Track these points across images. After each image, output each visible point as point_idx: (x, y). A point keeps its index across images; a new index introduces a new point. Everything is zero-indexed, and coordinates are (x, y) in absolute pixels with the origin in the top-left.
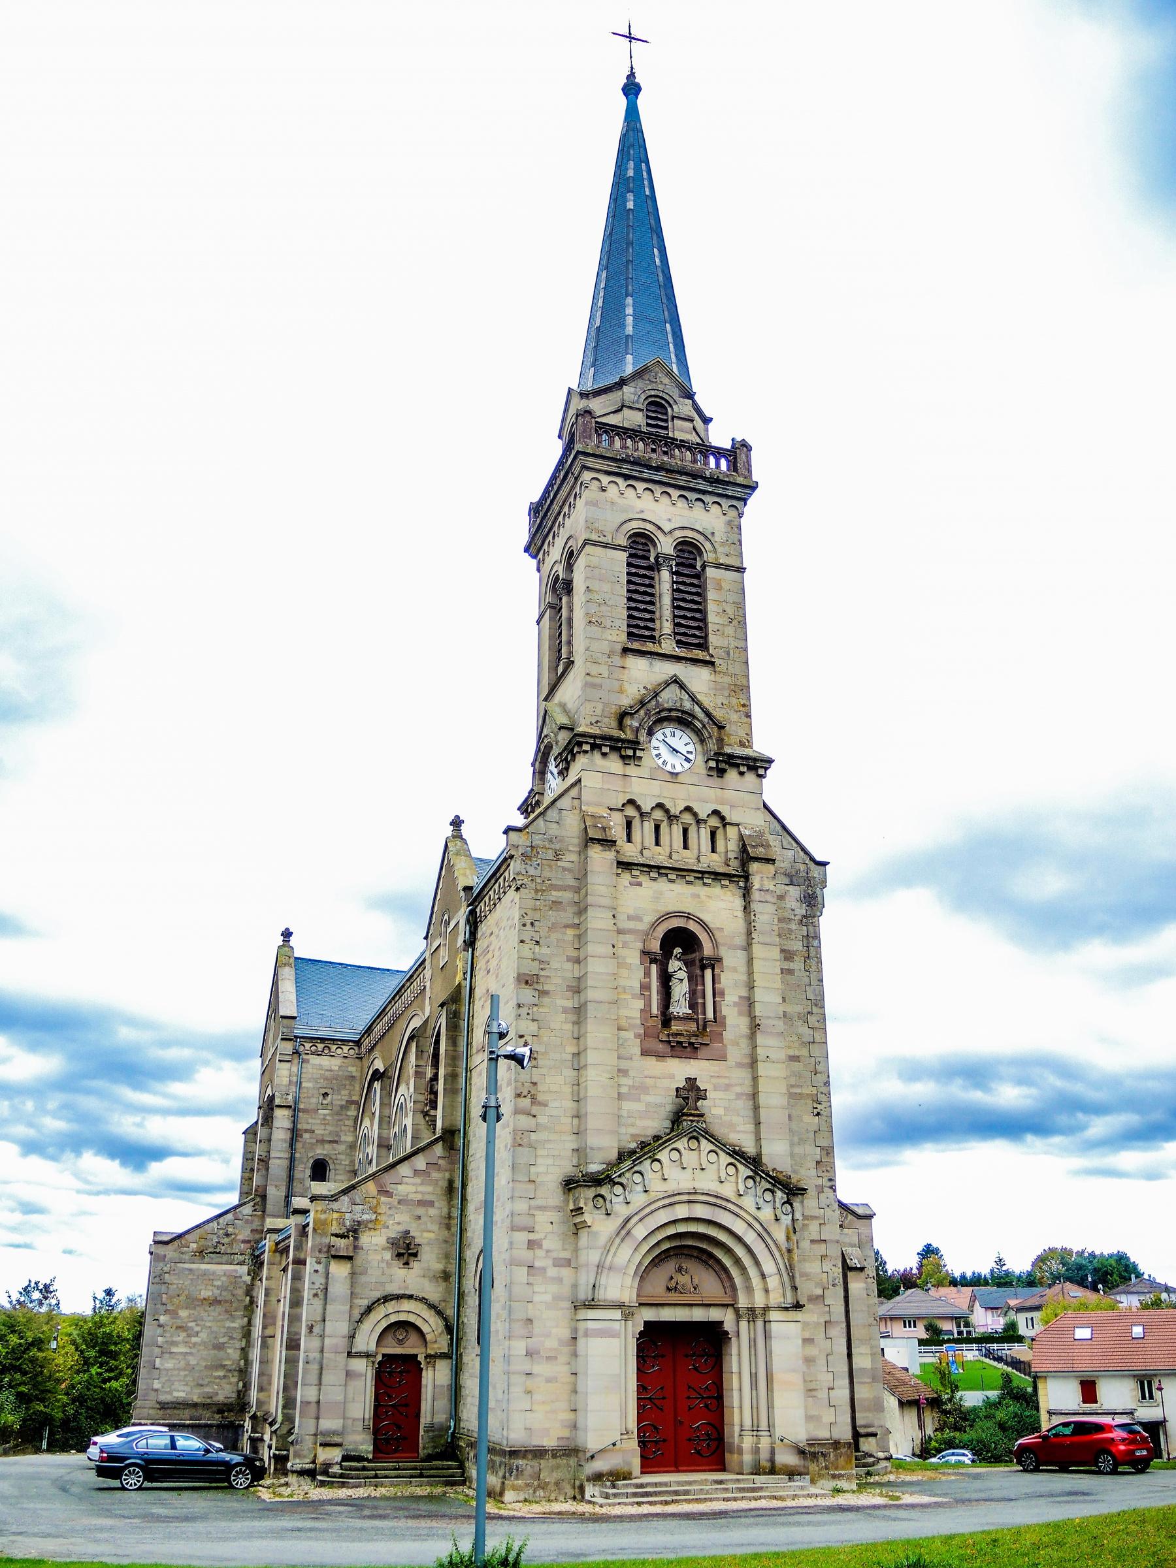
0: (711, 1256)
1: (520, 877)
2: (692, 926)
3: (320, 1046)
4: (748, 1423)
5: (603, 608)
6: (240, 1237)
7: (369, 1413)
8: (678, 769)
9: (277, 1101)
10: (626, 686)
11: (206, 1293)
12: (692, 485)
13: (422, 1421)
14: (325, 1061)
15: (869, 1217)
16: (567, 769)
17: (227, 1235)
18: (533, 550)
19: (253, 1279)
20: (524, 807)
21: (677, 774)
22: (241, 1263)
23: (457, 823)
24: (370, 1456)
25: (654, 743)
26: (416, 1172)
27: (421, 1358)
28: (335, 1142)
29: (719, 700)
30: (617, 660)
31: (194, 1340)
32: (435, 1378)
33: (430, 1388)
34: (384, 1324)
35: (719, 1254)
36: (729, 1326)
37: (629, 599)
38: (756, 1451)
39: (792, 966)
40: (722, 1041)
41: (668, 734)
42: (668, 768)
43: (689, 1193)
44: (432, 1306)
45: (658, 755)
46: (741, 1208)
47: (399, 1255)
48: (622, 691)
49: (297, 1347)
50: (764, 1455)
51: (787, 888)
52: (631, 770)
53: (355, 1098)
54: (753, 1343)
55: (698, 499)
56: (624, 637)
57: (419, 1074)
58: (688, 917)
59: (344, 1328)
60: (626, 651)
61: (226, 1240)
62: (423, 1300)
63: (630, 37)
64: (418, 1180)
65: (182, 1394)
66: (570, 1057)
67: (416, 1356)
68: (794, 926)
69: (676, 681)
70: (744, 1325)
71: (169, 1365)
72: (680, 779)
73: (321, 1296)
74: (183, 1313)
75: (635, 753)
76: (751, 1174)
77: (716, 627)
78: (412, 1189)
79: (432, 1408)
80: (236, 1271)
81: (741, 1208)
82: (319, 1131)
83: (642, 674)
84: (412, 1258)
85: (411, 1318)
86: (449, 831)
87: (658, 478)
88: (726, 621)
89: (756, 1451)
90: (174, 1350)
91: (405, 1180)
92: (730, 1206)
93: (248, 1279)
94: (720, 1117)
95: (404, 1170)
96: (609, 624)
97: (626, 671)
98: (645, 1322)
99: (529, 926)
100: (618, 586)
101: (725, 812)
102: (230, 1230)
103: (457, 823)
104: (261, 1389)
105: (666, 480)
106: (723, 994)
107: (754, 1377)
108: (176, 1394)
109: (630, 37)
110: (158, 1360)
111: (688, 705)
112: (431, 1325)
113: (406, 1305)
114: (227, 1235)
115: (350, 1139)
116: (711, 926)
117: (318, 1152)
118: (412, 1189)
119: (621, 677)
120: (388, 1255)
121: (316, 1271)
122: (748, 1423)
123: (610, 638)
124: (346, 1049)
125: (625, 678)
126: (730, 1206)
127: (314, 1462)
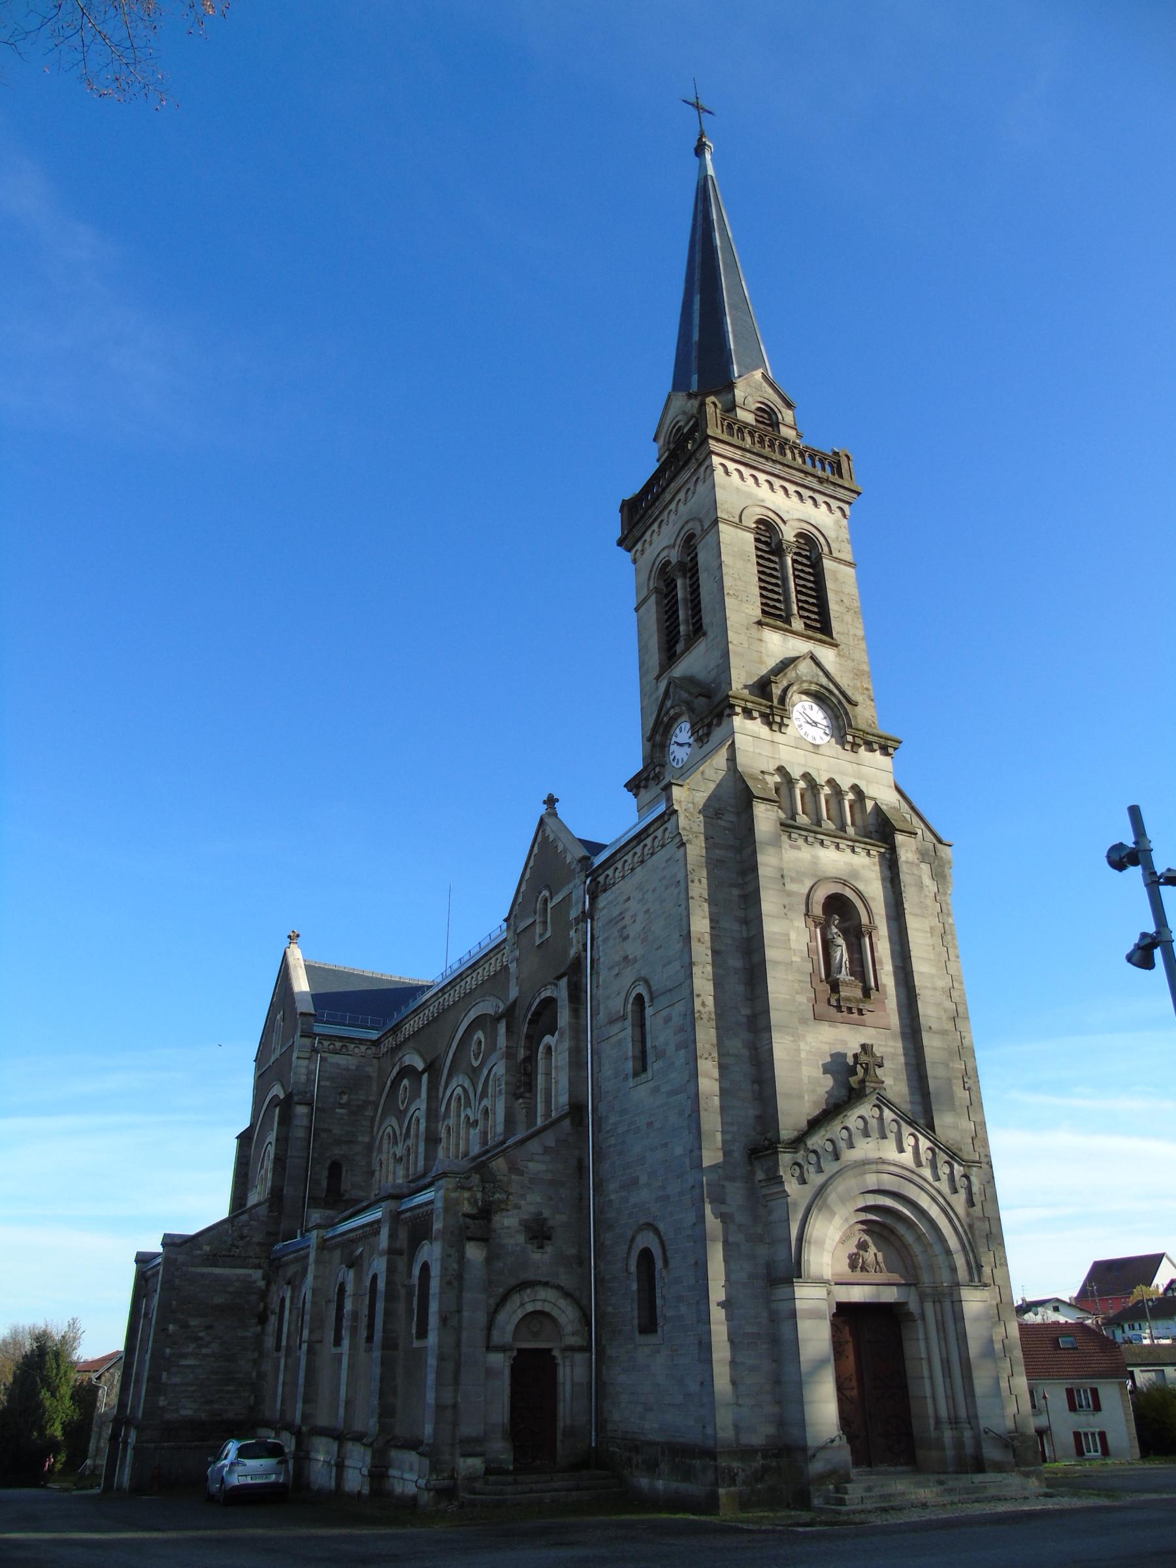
0: (892, 1231)
2: (848, 893)
3: (338, 1045)
4: (944, 1413)
5: (739, 583)
6: (255, 1240)
7: (507, 1419)
9: (296, 1099)
10: (765, 659)
11: (218, 1300)
12: (806, 483)
13: (560, 1424)
14: (341, 1060)
16: (708, 735)
17: (242, 1237)
18: (629, 542)
19: (268, 1285)
20: (633, 784)
21: (818, 746)
22: (258, 1267)
23: (551, 801)
24: (511, 1467)
26: (547, 1150)
27: (556, 1353)
28: (351, 1142)
31: (204, 1351)
32: (571, 1374)
33: (568, 1387)
34: (520, 1314)
35: (901, 1229)
36: (913, 1307)
37: (760, 580)
38: (959, 1444)
40: (885, 1010)
41: (807, 707)
44: (567, 1295)
45: (800, 726)
47: (533, 1238)
48: (761, 662)
49: (395, 1347)
50: (969, 1450)
52: (778, 737)
53: (372, 1098)
54: (941, 1326)
56: (759, 612)
57: (510, 1055)
58: (845, 883)
59: (481, 1317)
60: (760, 623)
61: (241, 1243)
62: (558, 1287)
63: (697, 106)
64: (547, 1158)
65: (190, 1412)
66: (744, 1020)
67: (550, 1350)
69: (813, 658)
70: (929, 1307)
71: (176, 1380)
72: (821, 751)
73: (456, 1284)
74: (193, 1322)
78: (543, 1167)
79: (569, 1406)
80: (250, 1275)
82: (337, 1130)
84: (546, 1242)
85: (547, 1308)
86: (542, 809)
87: (776, 472)
89: (959, 1444)
90: (184, 1362)
91: (536, 1157)
93: (262, 1284)
95: (534, 1146)
96: (745, 599)
100: (749, 565)
101: (863, 788)
102: (245, 1232)
103: (551, 801)
104: (306, 1400)
107: (946, 1363)
108: (183, 1412)
109: (697, 106)
110: (164, 1375)
111: (824, 681)
112: (566, 1314)
113: (543, 1293)
114: (242, 1237)
115: (367, 1139)
117: (336, 1151)
118: (543, 1167)
120: (521, 1239)
121: (449, 1256)
122: (944, 1413)
124: (363, 1048)
125: (763, 650)
127: (452, 1477)
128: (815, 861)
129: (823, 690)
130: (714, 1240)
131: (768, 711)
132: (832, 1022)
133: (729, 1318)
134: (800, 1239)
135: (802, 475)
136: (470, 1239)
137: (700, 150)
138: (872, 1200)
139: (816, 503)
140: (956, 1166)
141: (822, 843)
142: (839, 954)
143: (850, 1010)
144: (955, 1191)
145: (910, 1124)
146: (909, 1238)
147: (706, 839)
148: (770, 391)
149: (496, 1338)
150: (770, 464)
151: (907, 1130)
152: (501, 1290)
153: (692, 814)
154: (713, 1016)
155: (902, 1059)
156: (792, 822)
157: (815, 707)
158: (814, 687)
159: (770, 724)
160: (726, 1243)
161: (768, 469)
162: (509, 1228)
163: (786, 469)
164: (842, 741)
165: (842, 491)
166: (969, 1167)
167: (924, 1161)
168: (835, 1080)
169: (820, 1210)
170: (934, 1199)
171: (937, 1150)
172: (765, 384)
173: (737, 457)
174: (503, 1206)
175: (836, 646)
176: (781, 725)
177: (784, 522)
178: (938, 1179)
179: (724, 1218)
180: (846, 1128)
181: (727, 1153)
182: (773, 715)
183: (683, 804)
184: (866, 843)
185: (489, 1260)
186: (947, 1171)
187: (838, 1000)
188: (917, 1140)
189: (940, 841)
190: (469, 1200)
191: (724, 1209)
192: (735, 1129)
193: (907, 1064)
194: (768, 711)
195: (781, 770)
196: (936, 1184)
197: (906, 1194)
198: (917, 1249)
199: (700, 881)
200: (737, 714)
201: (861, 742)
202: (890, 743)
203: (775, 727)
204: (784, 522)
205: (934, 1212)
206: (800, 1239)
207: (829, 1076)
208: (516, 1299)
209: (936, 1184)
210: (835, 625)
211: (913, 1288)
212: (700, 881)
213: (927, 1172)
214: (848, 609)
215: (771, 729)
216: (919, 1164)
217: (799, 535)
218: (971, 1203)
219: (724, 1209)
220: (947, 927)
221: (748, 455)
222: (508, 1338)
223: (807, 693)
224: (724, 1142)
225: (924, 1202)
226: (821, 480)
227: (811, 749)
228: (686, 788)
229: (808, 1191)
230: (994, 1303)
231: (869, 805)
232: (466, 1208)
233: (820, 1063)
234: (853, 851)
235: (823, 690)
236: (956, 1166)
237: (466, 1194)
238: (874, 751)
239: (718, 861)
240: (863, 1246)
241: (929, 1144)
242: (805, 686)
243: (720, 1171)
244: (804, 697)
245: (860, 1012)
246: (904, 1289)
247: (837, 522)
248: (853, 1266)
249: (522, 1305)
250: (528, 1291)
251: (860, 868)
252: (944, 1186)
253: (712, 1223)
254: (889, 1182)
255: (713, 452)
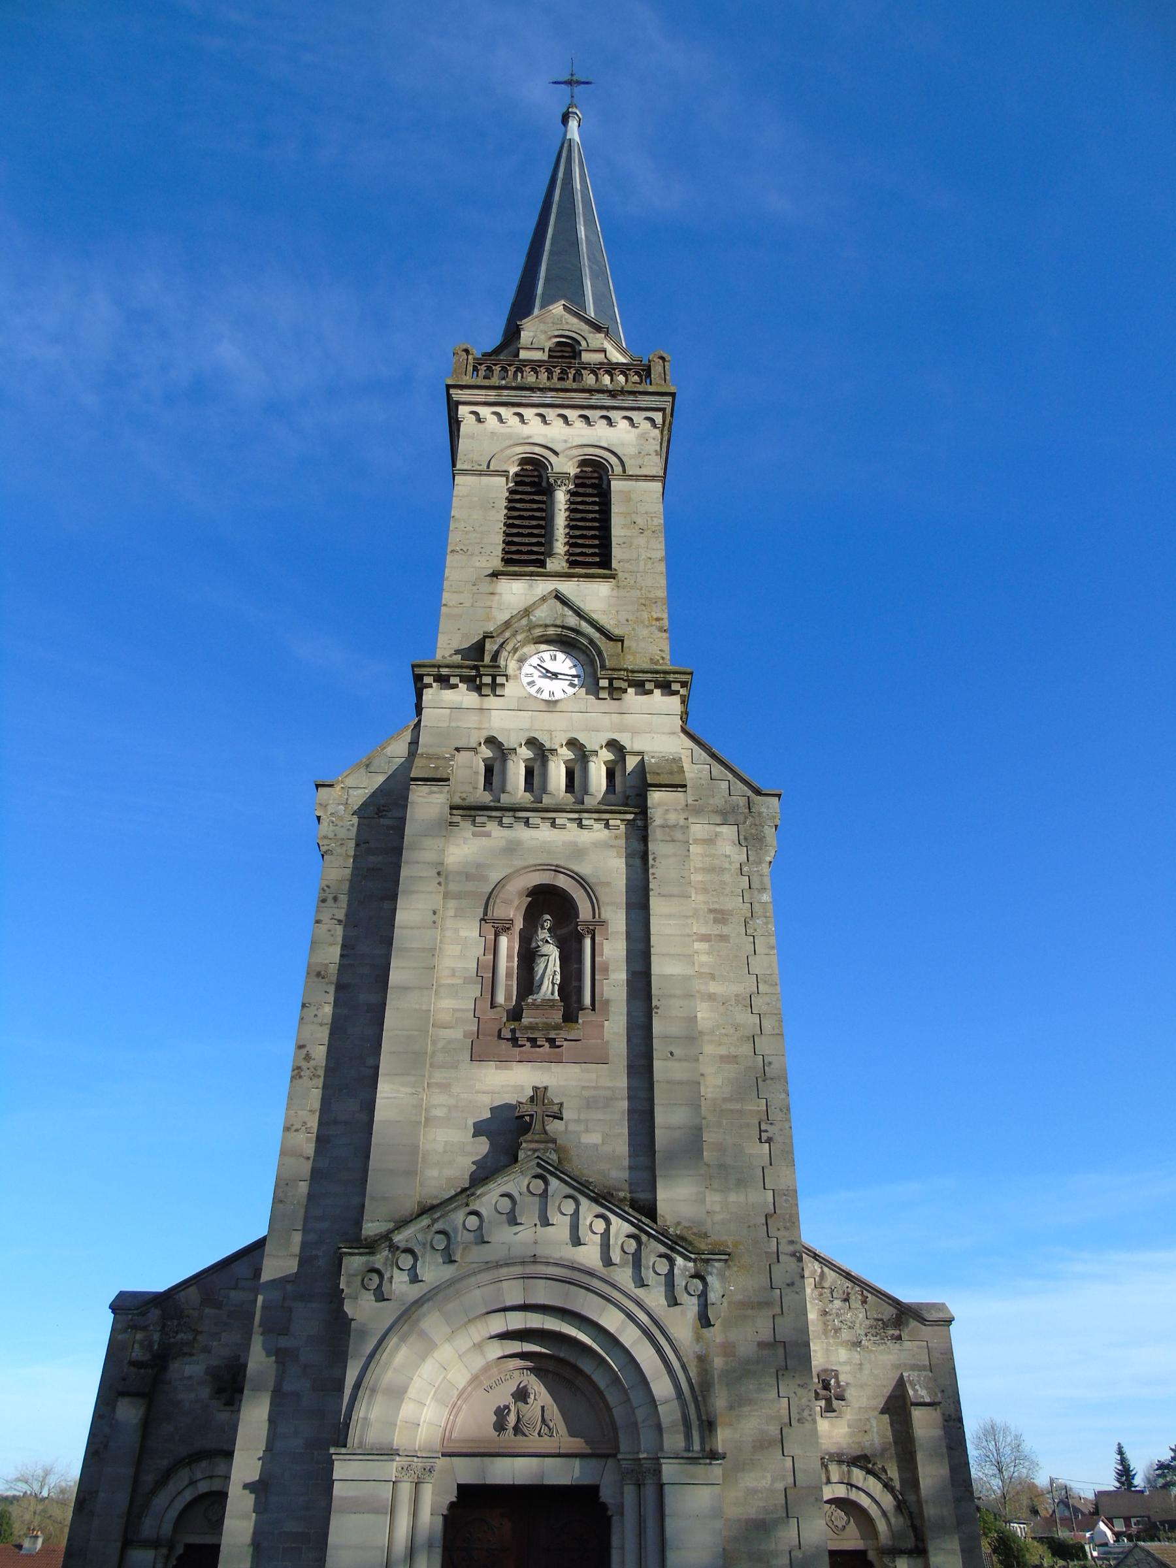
1: (326, 842)
2: (562, 882)
8: (559, 695)
12: (593, 402)
15: (949, 1321)
21: (556, 701)
25: (527, 668)
27: (872, 1556)
29: (623, 617)
30: (486, 586)
34: (188, 1496)
35: (586, 1366)
39: (726, 930)
42: (545, 696)
43: (523, 1263)
45: (532, 683)
46: (614, 1286)
48: (488, 618)
51: (718, 829)
52: (492, 702)
55: (603, 417)
58: (557, 870)
68: (727, 877)
69: (560, 598)
70: (629, 1491)
72: (560, 707)
75: (494, 680)
76: (632, 1230)
77: (621, 541)
81: (614, 1286)
83: (517, 593)
87: (548, 401)
88: (636, 532)
92: (596, 1283)
94: (596, 1146)
97: (496, 598)
98: (461, 1488)
99: (330, 902)
105: (559, 401)
106: (606, 970)
111: (572, 620)
116: (591, 880)
119: (488, 603)
120: (205, 1392)
123: (478, 564)
126: (596, 1283)
128: (512, 849)
129: (566, 632)
130: (257, 1389)
131: (473, 673)
132: (503, 1060)
133: (259, 1508)
134: (357, 1386)
135: (586, 395)
136: (123, 1394)
137: (565, 119)
138: (517, 1321)
139: (610, 421)
140: (680, 1261)
141: (527, 823)
142: (542, 966)
143: (533, 1041)
144: (673, 1302)
145: (595, 1200)
146: (601, 1381)
147: (357, 845)
148: (575, 320)
149: (147, 1527)
150: (538, 394)
151: (588, 1210)
152: (165, 1462)
153: (341, 818)
154: (321, 1072)
155: (625, 1105)
156: (582, 807)
157: (561, 656)
158: (551, 631)
159: (478, 689)
160: (278, 1397)
161: (536, 400)
162: (190, 1377)
163: (562, 394)
164: (593, 689)
165: (647, 398)
166: (707, 1261)
167: (616, 1256)
168: (491, 1144)
169: (403, 1339)
170: (630, 1316)
171: (644, 1238)
172: (567, 316)
173: (492, 399)
174: (186, 1350)
175: (613, 577)
176: (494, 686)
177: (556, 453)
178: (641, 1283)
179: (282, 1357)
180: (476, 1213)
181: (304, 1261)
182: (481, 676)
183: (330, 809)
184: (620, 812)
185: (146, 1425)
186: (663, 1267)
187: (513, 1031)
188: (608, 1222)
189: (758, 792)
190: (141, 1343)
191: (284, 1342)
192: (325, 1225)
193: (631, 1112)
194: (473, 673)
195: (491, 741)
196: (640, 1293)
197: (578, 1310)
198: (612, 1398)
199: (335, 899)
200: (430, 686)
201: (624, 685)
202: (671, 677)
203: (485, 691)
204: (556, 453)
205: (630, 1337)
206: (357, 1386)
207: (484, 1139)
208: (184, 1475)
209: (640, 1293)
210: (616, 552)
211: (610, 1462)
212: (335, 899)
213: (624, 1276)
214: (642, 531)
215: (481, 695)
216: (608, 1262)
217: (583, 463)
218: (704, 1320)
219: (284, 1342)
220: (756, 907)
221: (505, 392)
222: (167, 1528)
223: (547, 641)
224: (304, 1245)
225: (612, 1320)
226: (613, 394)
227: (543, 707)
228: (338, 788)
229: (387, 1313)
230: (780, 1486)
231: (631, 763)
232: (137, 1354)
233: (470, 1122)
234: (581, 826)
235: (566, 632)
236: (680, 1261)
237: (139, 1336)
238: (650, 692)
239: (369, 870)
240: (521, 1395)
241: (627, 1228)
242: (538, 632)
243: (289, 1287)
244: (543, 647)
245: (552, 1042)
246: (593, 1462)
247: (644, 437)
248: (500, 1426)
249: (192, 1483)
250: (204, 1464)
251: (593, 850)
252: (655, 1298)
253: (258, 1360)
254: (543, 1294)
255: (458, 403)
